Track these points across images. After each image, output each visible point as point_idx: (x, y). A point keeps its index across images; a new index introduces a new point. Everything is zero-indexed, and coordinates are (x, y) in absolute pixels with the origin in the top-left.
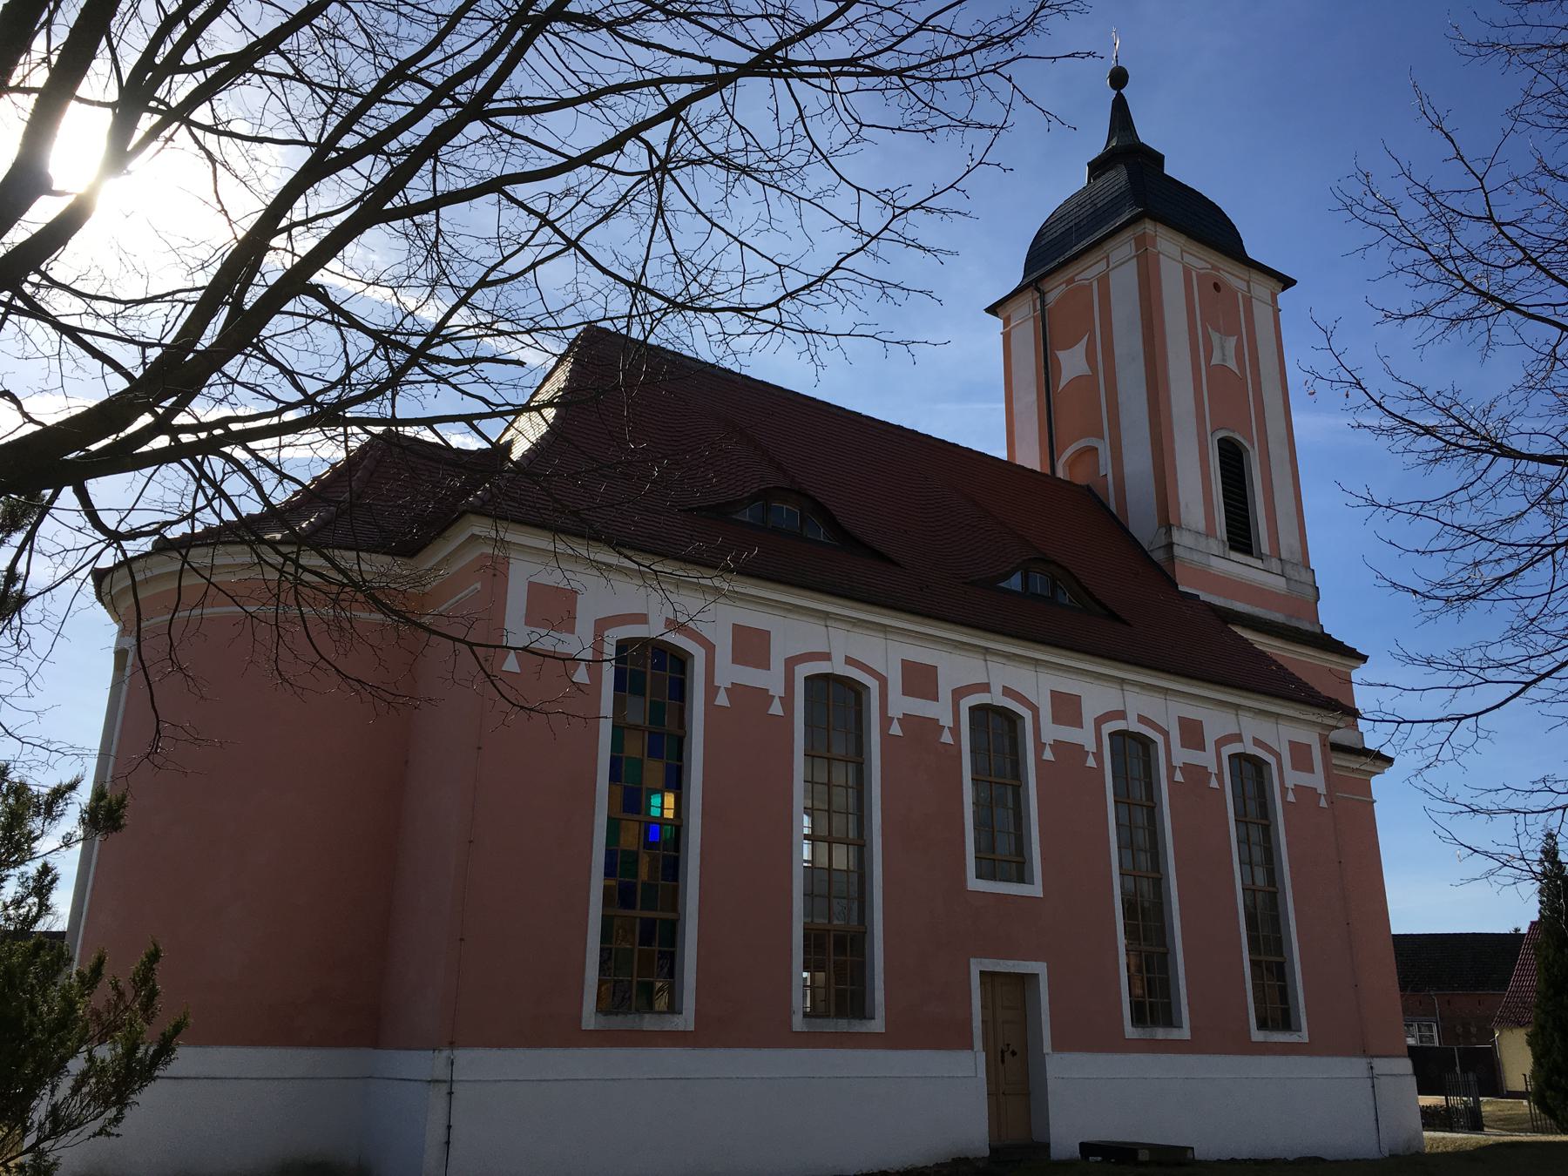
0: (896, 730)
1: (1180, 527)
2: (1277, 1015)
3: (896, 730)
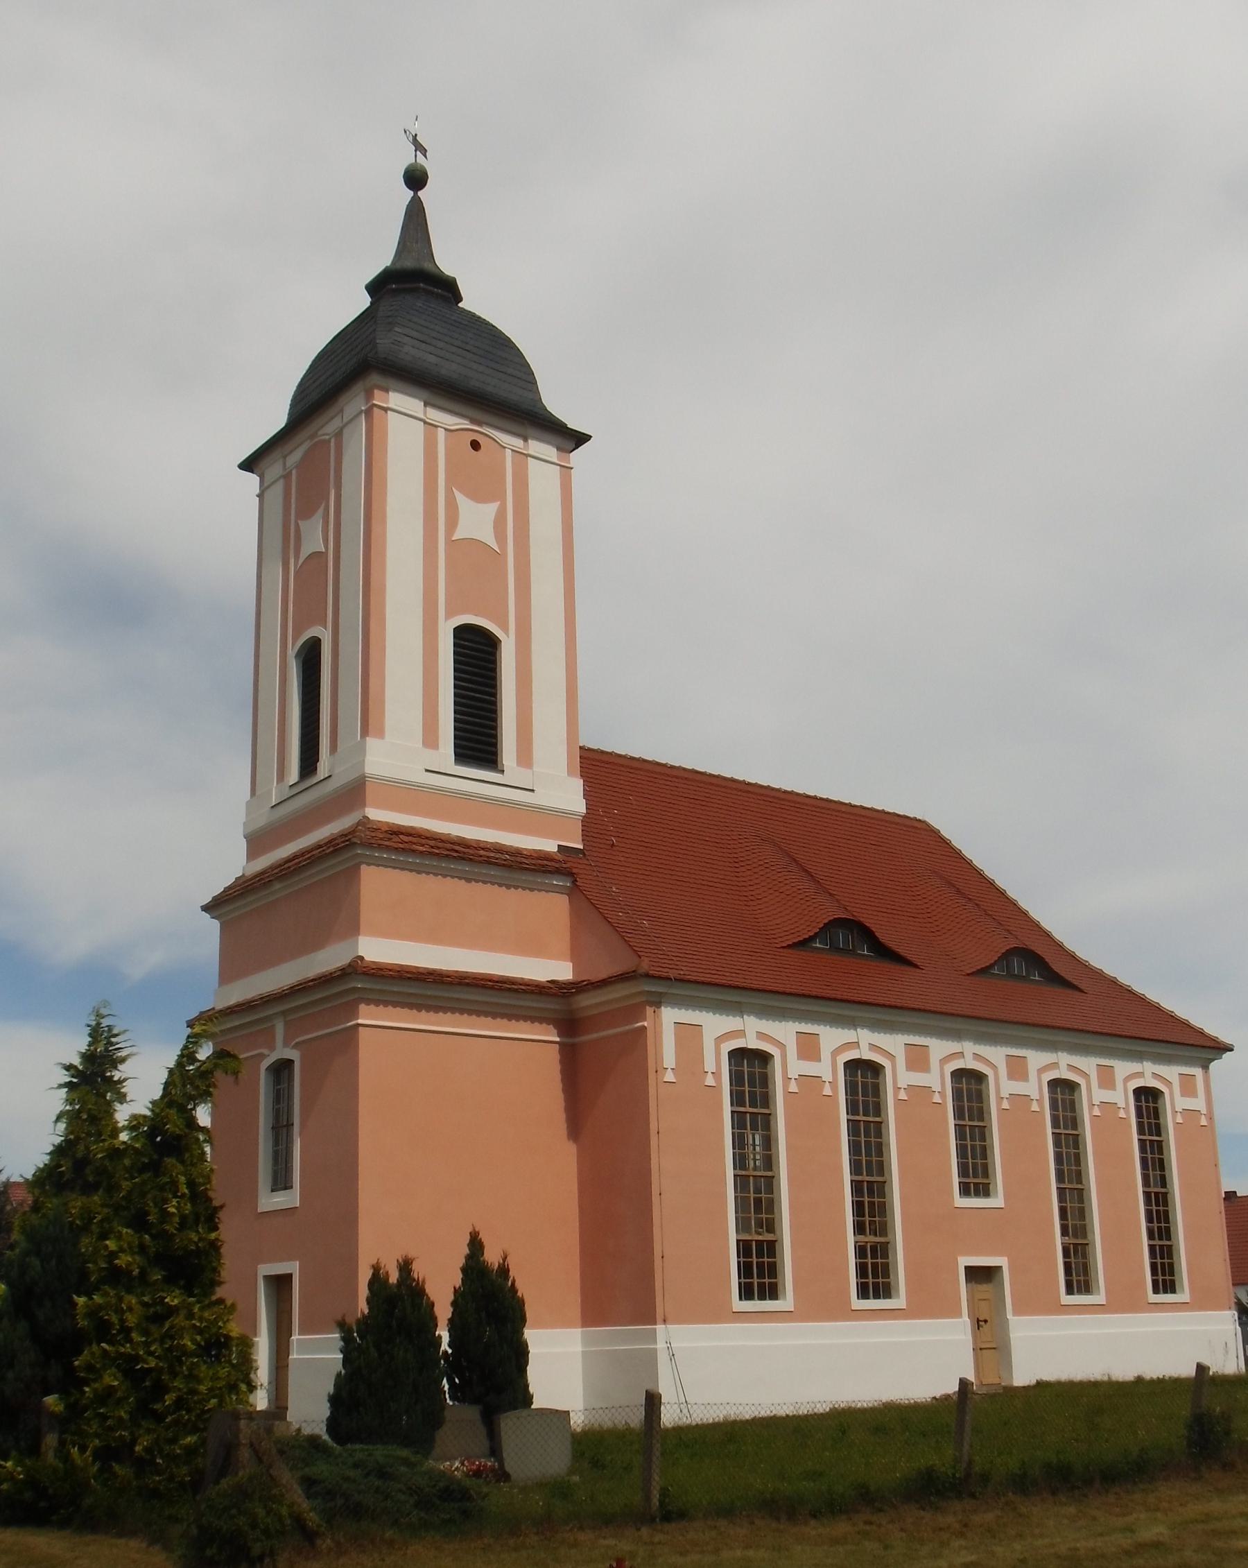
0: (1005, 1105)
2: (1165, 1279)
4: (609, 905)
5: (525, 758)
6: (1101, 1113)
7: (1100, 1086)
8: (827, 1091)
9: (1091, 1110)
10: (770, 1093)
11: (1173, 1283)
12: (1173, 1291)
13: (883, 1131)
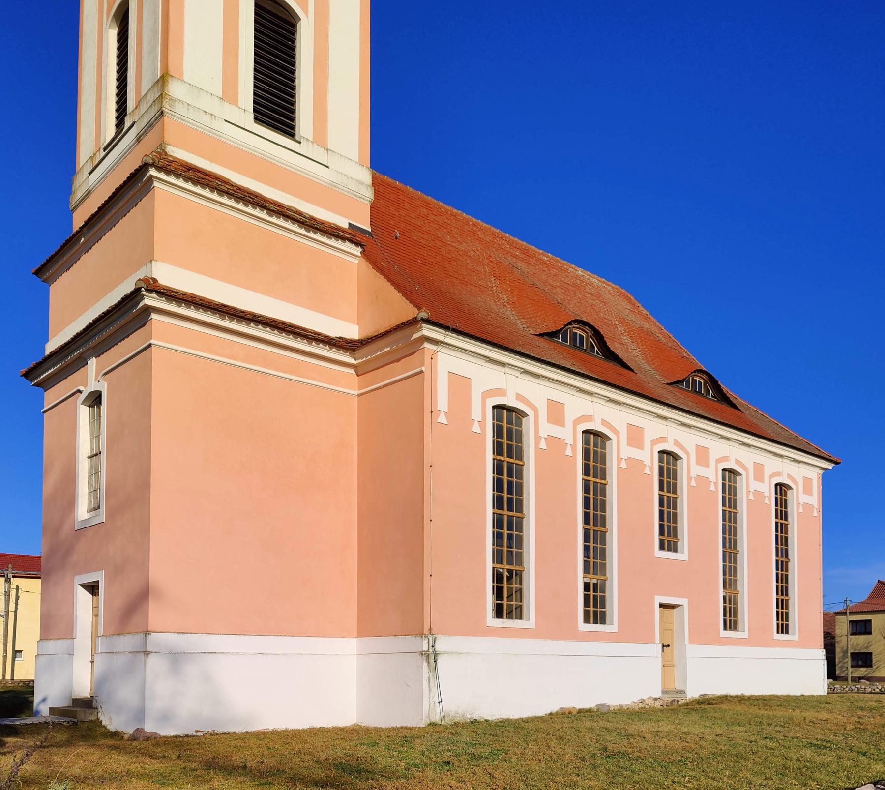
1: (181, 79)
2: (731, 623)
3: (624, 465)
4: (379, 232)
5: (320, 139)
6: (627, 467)
7: (629, 444)
8: (569, 452)
9: (748, 495)
10: (524, 449)
11: (603, 614)
12: (603, 622)
13: (524, 473)
